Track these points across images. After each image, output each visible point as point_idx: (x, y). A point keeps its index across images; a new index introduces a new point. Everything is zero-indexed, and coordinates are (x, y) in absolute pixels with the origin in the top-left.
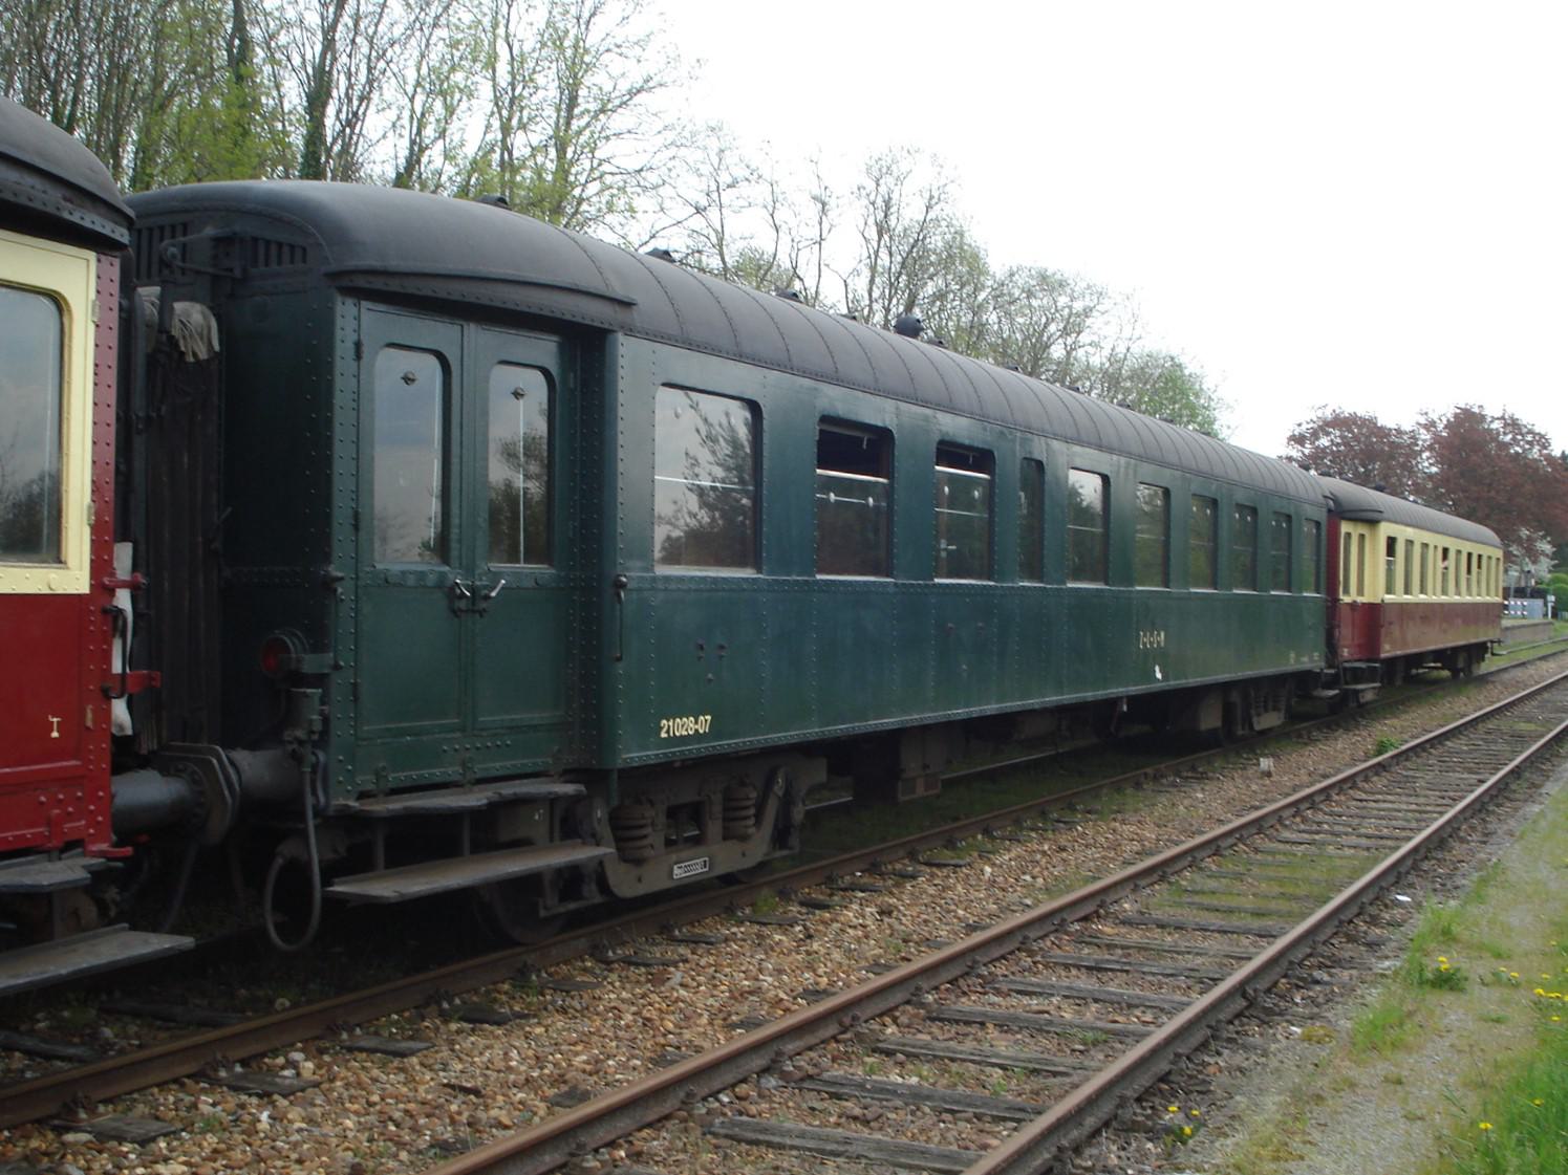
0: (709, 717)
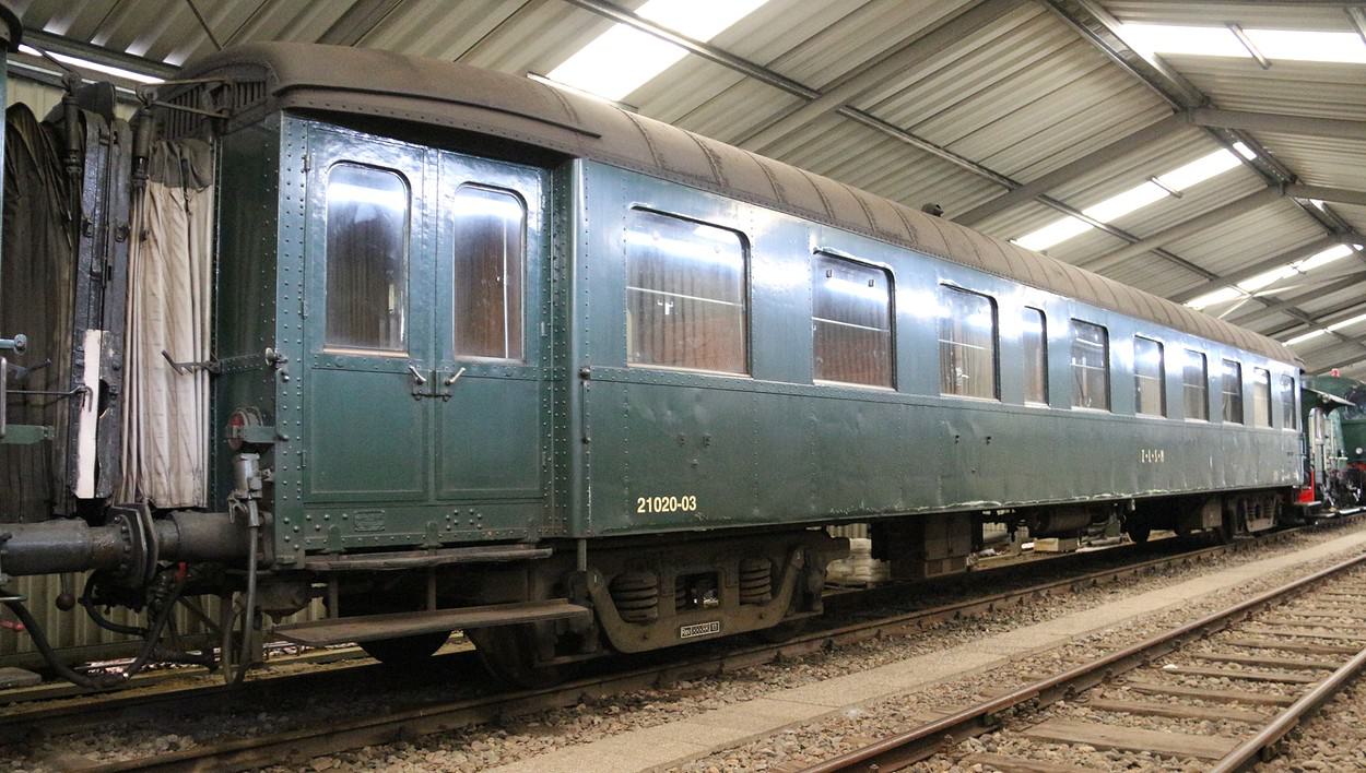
0: (640, 510)
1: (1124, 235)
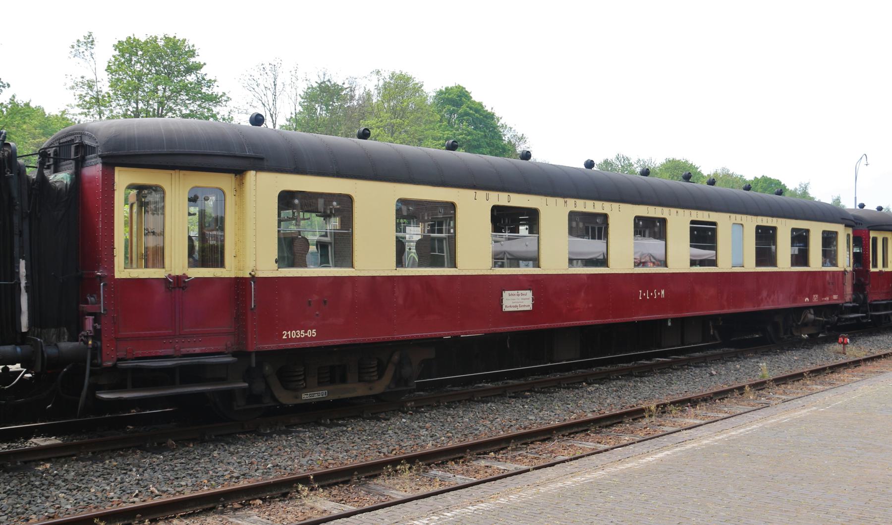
0: (284, 337)
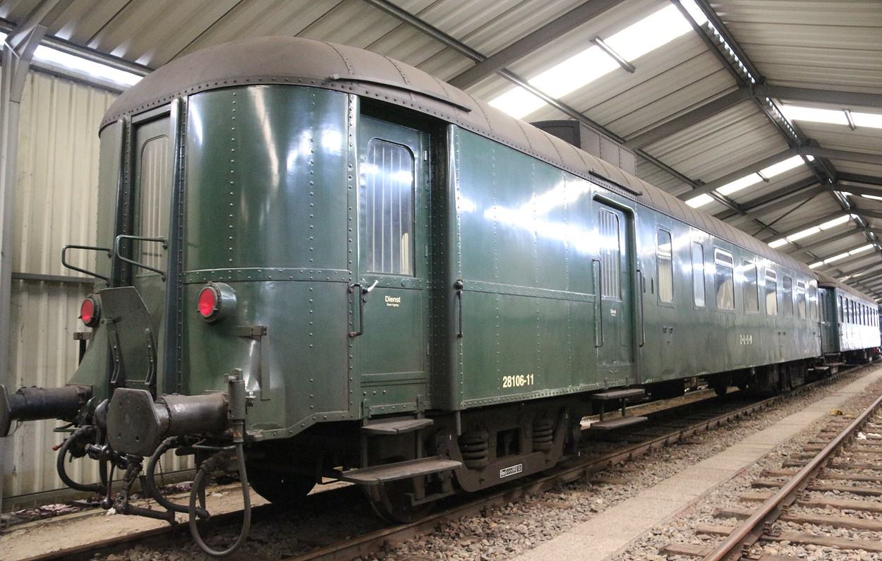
0: (504, 386)
1: (797, 246)
